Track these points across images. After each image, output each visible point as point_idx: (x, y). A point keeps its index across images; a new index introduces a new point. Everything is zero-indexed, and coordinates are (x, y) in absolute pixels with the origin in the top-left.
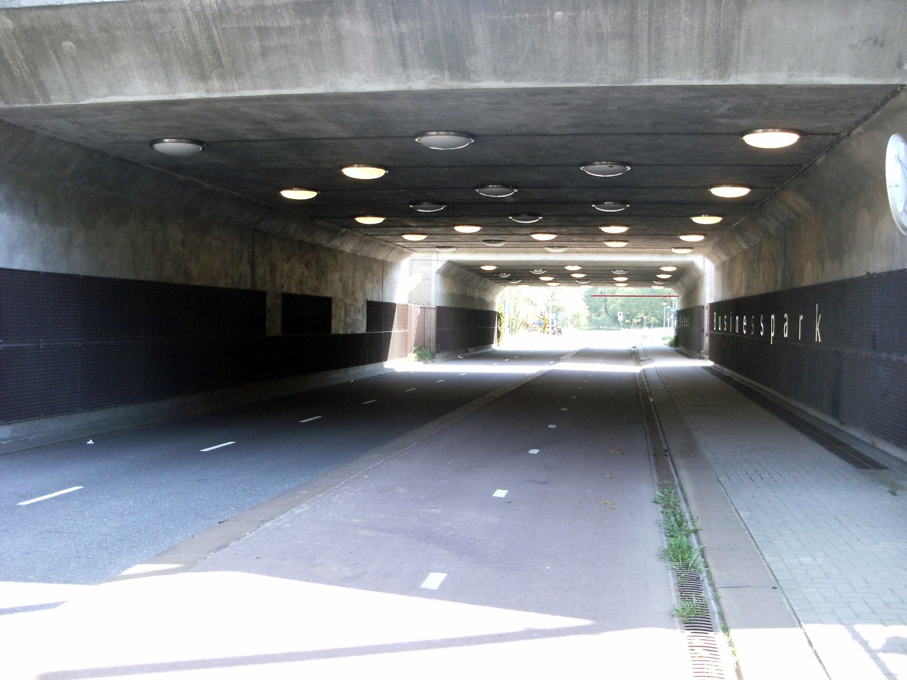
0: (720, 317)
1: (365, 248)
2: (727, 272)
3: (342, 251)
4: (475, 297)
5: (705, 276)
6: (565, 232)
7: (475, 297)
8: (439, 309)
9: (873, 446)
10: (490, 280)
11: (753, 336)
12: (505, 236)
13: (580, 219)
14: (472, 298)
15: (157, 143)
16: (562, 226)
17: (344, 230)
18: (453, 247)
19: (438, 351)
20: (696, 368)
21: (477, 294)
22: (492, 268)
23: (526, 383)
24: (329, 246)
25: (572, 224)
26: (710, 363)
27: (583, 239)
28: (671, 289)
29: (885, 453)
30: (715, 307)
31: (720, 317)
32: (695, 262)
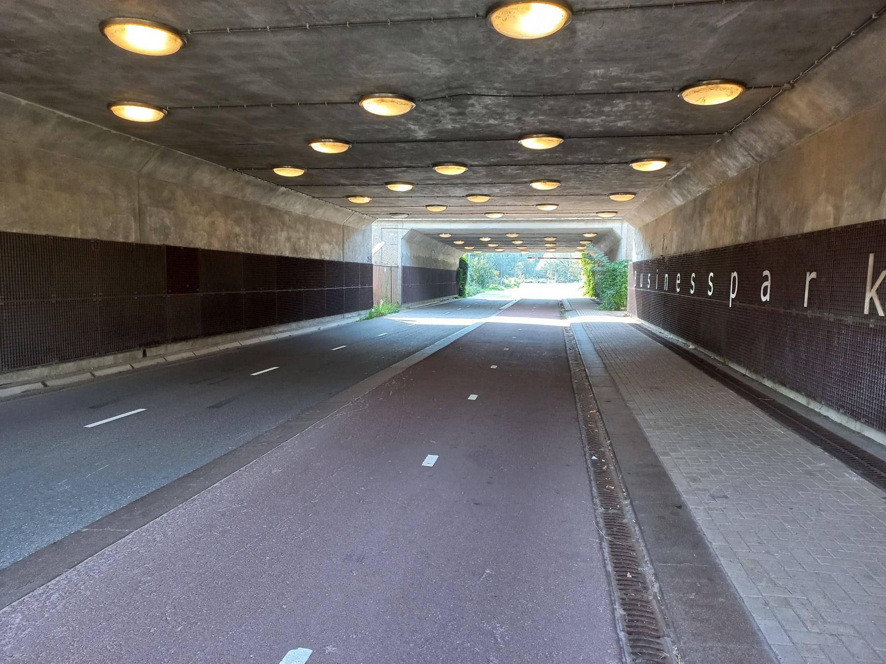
0: (642, 275)
1: (318, 211)
2: (649, 232)
3: (290, 212)
4: (439, 260)
5: (622, 240)
6: (498, 193)
7: (439, 260)
8: (404, 268)
9: (724, 364)
10: (452, 246)
11: (693, 295)
12: (444, 199)
13: (510, 170)
14: (436, 261)
15: (114, 106)
16: (492, 184)
17: (283, 189)
18: (404, 214)
19: (404, 301)
20: (622, 325)
21: (441, 257)
22: (448, 236)
23: (454, 345)
24: (269, 204)
25: (501, 181)
26: (635, 320)
27: (516, 203)
28: (634, 228)
29: (732, 368)
30: (639, 266)
31: (642, 275)
32: (614, 229)
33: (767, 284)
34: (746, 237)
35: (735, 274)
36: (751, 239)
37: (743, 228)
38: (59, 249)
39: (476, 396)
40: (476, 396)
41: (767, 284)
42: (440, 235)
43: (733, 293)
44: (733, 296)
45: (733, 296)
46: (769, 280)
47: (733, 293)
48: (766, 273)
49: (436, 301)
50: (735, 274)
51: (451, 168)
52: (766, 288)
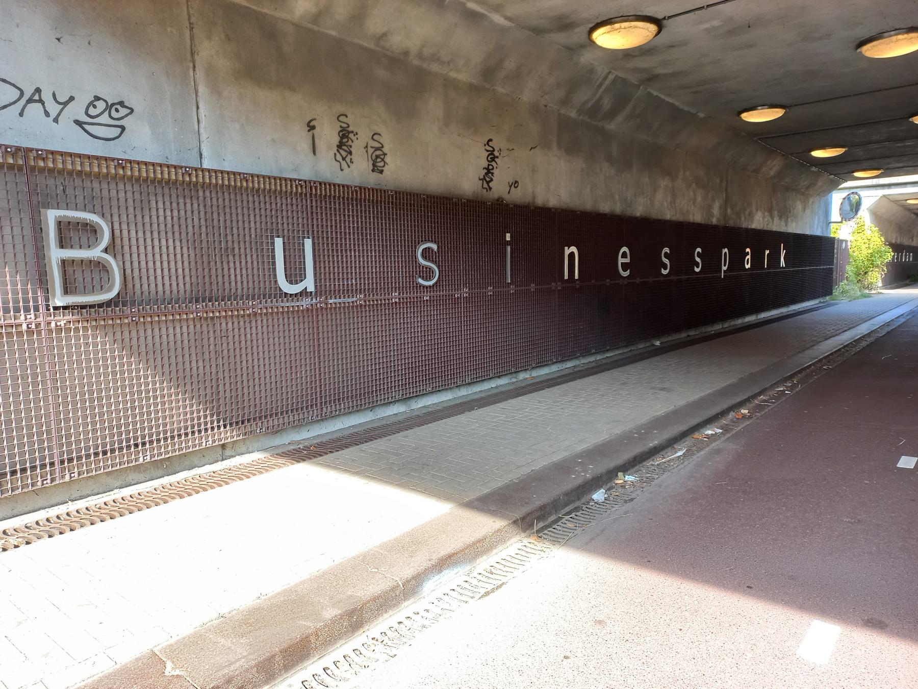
33: (749, 257)
34: (718, 220)
35: (726, 250)
36: (722, 223)
37: (716, 211)
38: (340, 221)
39: (900, 465)
40: (900, 465)
41: (749, 257)
42: (908, 201)
43: (725, 266)
44: (724, 268)
45: (724, 268)
46: (629, 257)
47: (725, 266)
48: (748, 250)
49: (870, 340)
50: (726, 250)
51: (897, 40)
52: (748, 259)
